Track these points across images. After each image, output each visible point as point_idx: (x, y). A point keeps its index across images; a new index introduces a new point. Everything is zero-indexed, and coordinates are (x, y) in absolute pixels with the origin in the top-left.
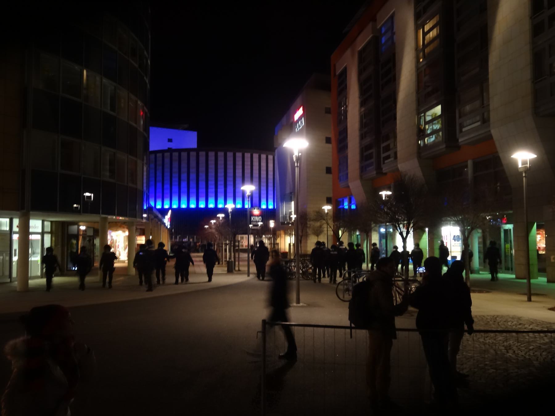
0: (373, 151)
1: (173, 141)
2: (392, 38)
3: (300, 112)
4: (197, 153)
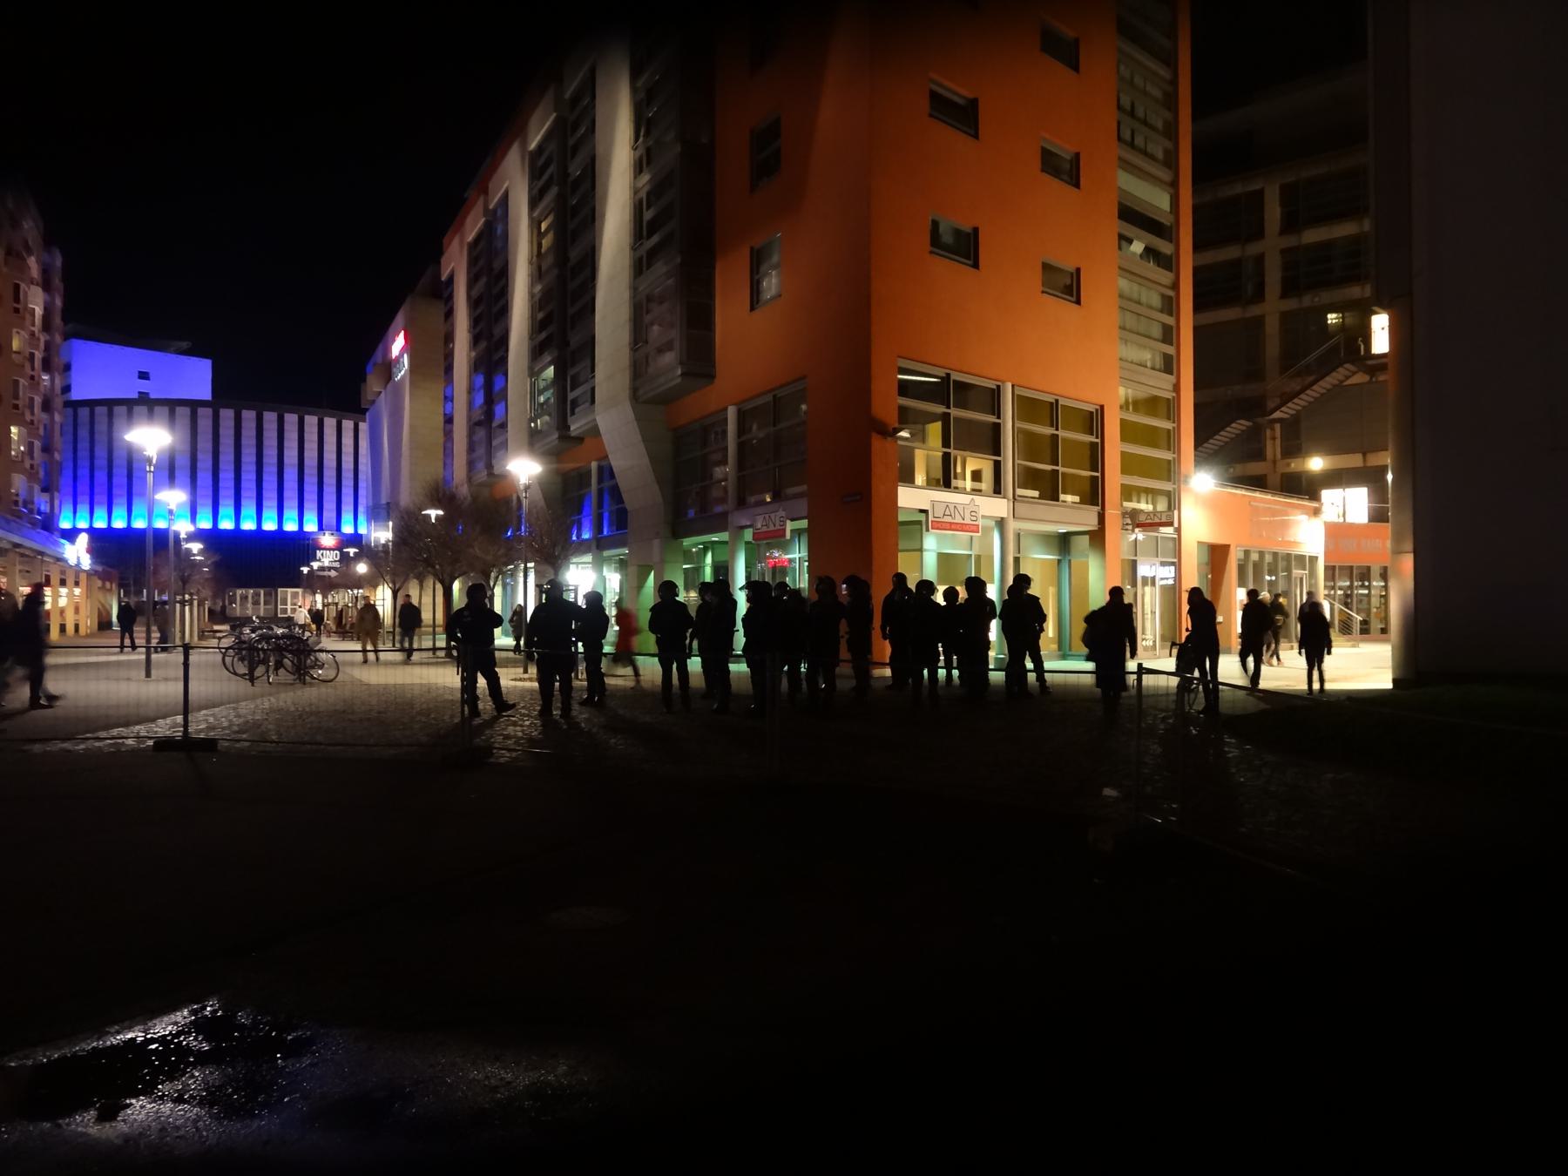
2: (635, 244)
4: (214, 411)
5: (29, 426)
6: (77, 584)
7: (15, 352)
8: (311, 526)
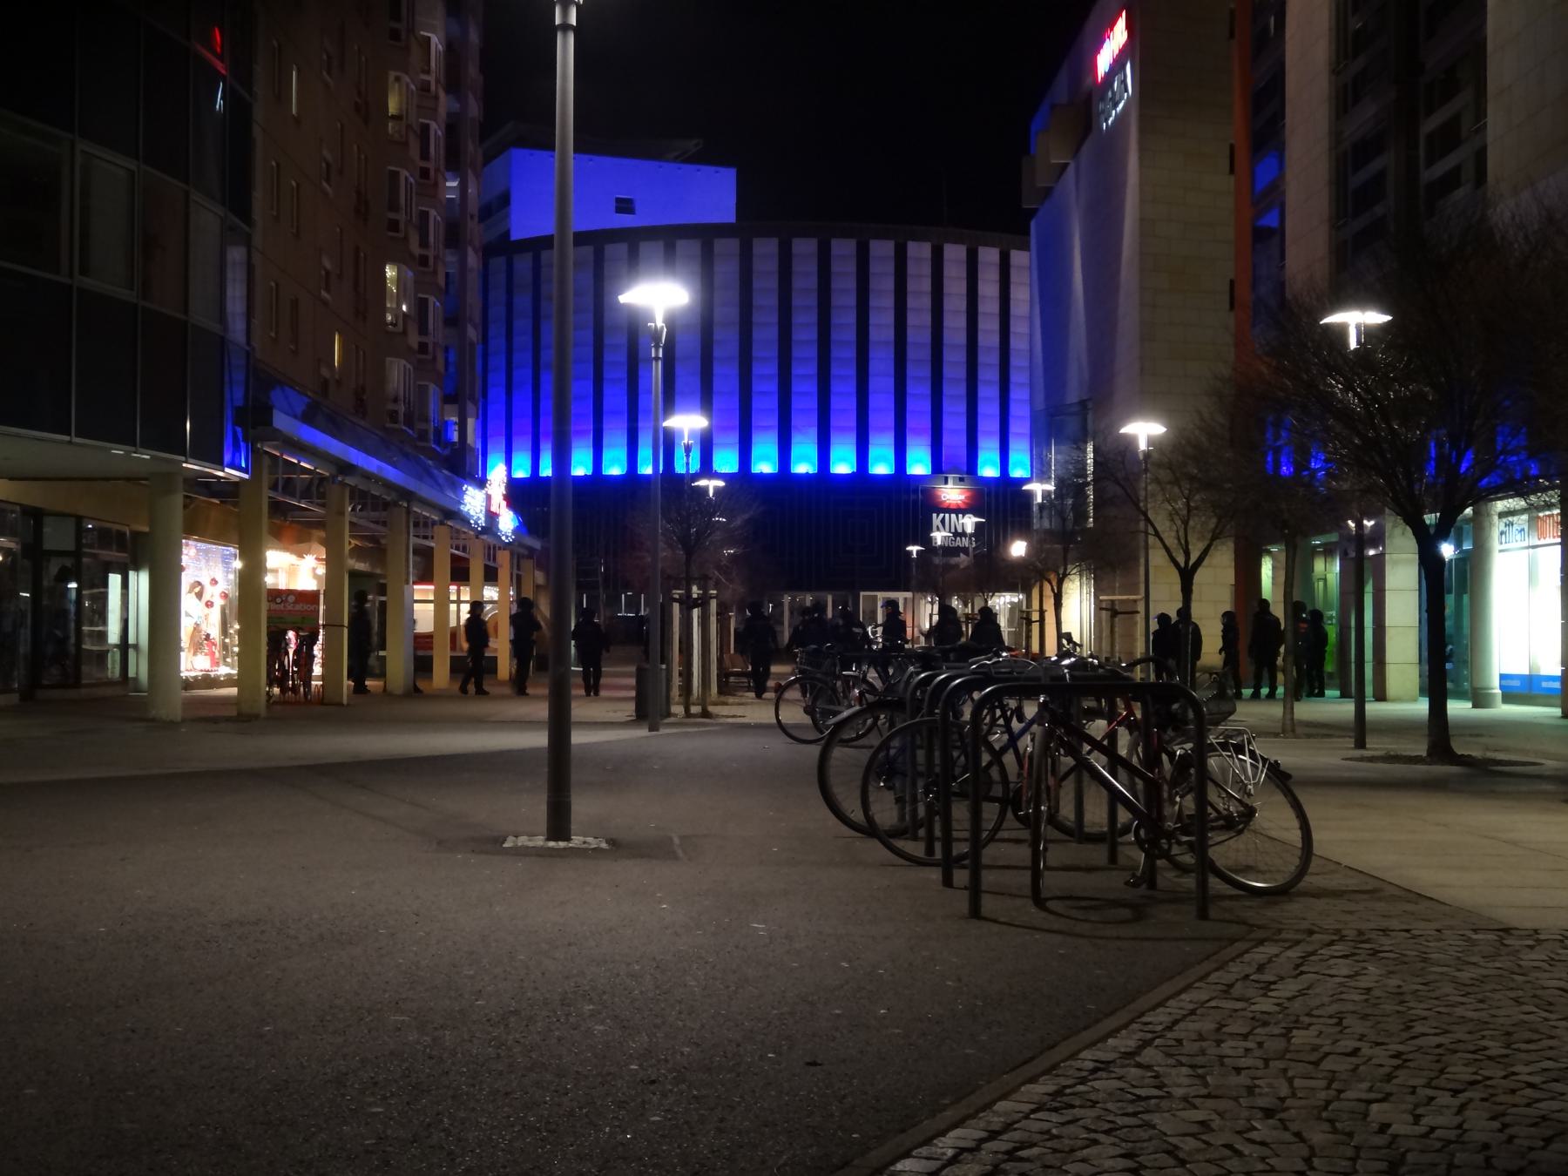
0: (1386, 161)
1: (638, 208)
3: (1119, 36)
5: (419, 264)
6: (491, 576)
7: (393, 117)
8: (919, 464)
